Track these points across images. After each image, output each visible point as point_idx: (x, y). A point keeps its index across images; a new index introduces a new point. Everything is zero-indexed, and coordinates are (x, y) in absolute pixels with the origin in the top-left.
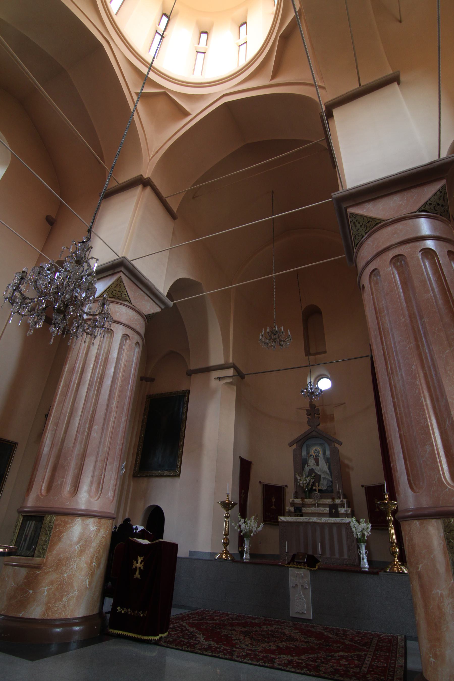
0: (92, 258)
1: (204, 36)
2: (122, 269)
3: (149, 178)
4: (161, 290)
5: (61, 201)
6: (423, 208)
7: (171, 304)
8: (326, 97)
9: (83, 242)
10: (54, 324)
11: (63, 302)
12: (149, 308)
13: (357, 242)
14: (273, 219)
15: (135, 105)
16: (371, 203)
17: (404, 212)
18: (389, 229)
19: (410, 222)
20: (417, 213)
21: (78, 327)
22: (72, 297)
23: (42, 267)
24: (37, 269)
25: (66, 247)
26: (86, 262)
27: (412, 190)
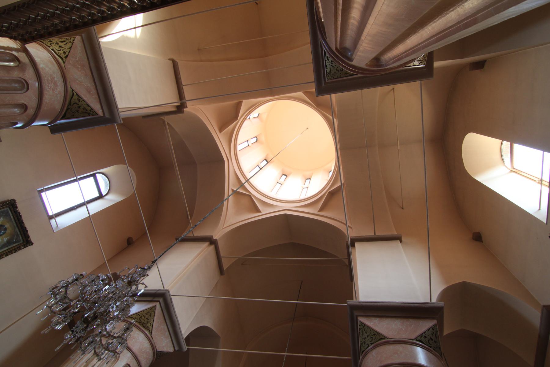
0: (143, 284)
1: (284, 177)
2: (161, 300)
3: (216, 240)
4: (183, 332)
5: (146, 232)
6: (419, 338)
7: (185, 348)
8: (352, 233)
9: (144, 269)
10: (73, 331)
11: (95, 313)
12: (164, 345)
13: (362, 348)
14: (297, 303)
15: (229, 196)
16: (377, 319)
17: (404, 336)
18: (392, 347)
19: (408, 346)
20: (414, 341)
21: (92, 342)
22: (105, 311)
23: (98, 276)
24: (93, 277)
25: (127, 268)
26: (136, 285)
27: (410, 320)
